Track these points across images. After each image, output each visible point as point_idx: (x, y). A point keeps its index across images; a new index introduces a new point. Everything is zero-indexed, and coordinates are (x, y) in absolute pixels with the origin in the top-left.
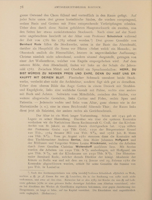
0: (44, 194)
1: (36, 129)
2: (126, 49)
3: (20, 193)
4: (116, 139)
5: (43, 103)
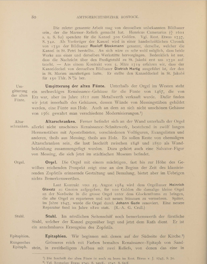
0: (80, 108)
1: (70, 167)
2: (156, 108)
3: (183, 217)
4: (131, 68)
5: (115, 133)
